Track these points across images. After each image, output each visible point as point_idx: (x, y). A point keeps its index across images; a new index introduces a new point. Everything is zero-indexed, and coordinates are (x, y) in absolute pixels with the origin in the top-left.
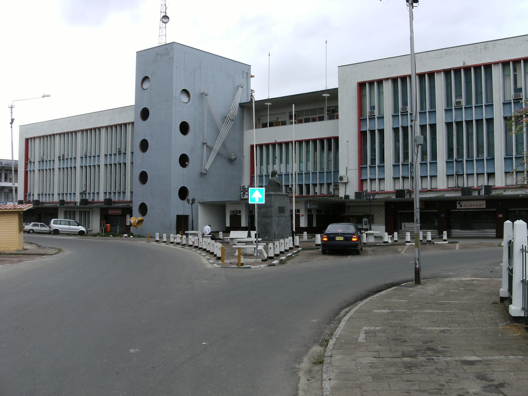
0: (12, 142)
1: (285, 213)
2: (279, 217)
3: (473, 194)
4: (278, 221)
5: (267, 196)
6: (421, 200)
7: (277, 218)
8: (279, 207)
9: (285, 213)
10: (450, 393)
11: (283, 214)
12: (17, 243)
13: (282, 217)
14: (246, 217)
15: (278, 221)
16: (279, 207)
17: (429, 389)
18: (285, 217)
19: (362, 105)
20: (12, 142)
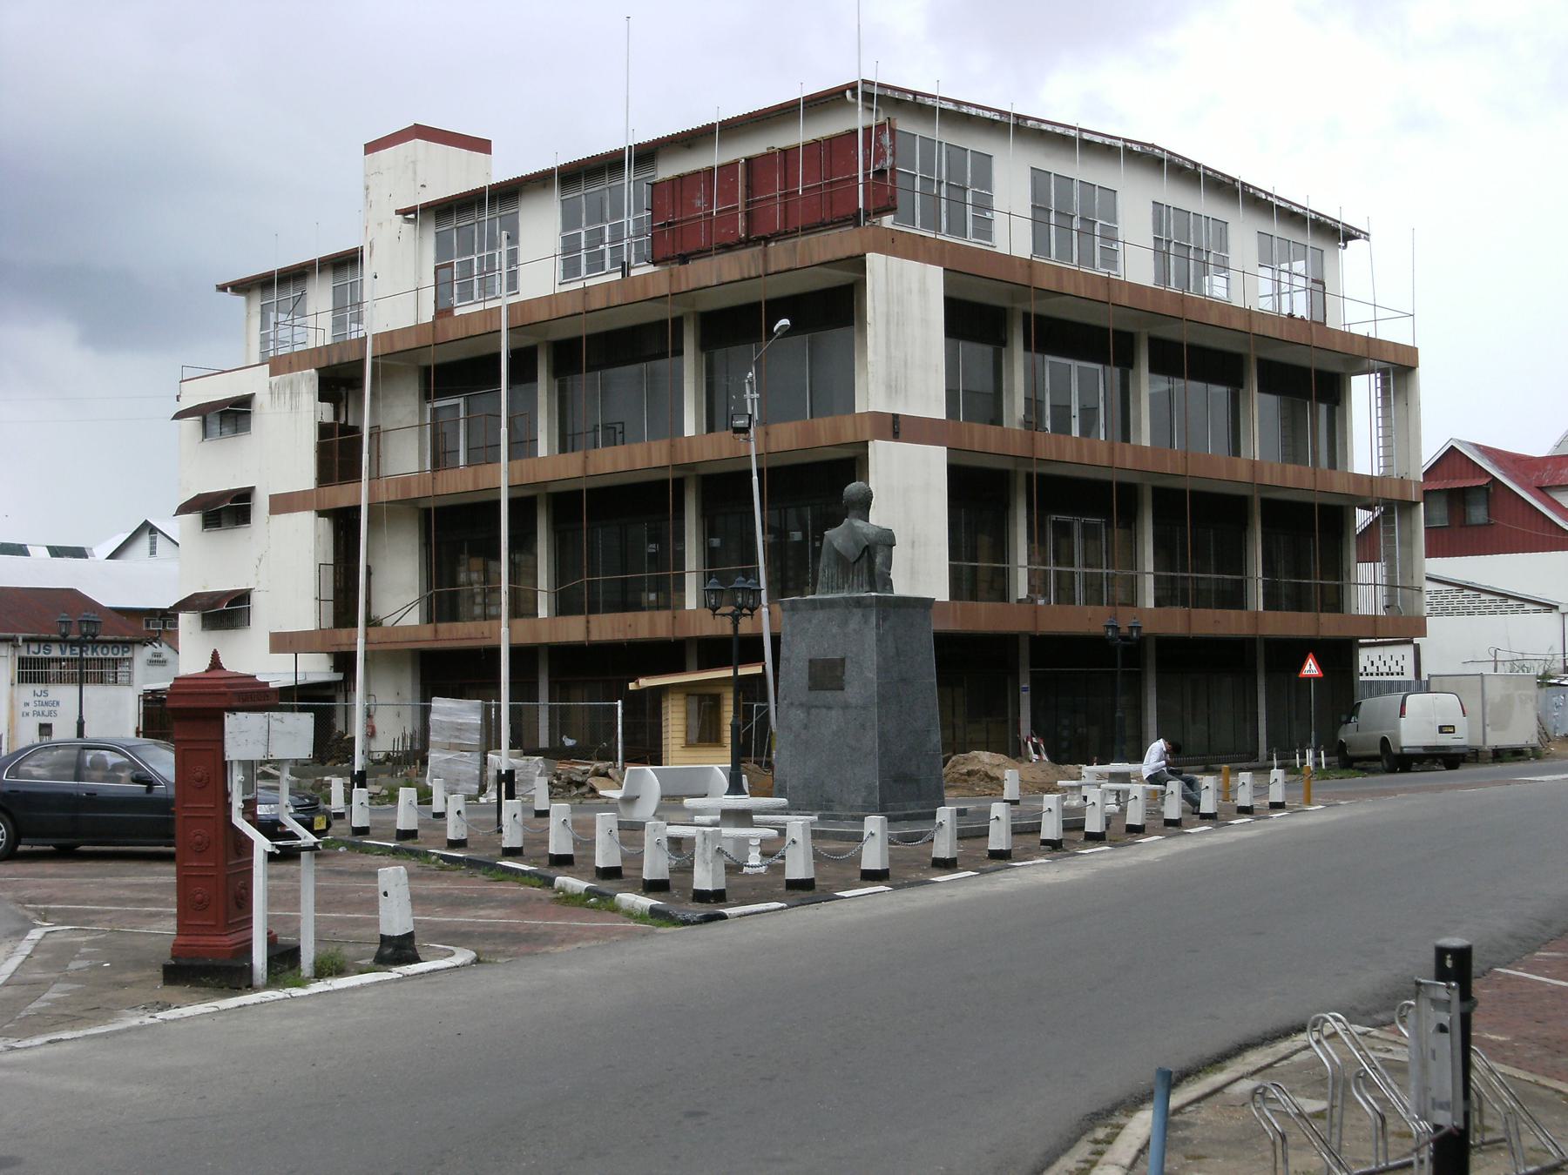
0: (628, 97)
1: (848, 689)
2: (808, 707)
3: (1272, 400)
4: (806, 727)
5: (721, 543)
6: (565, 605)
7: (800, 714)
8: (810, 661)
9: (843, 689)
10: (865, 1020)
11: (829, 696)
12: (673, 725)
13: (829, 708)
14: (413, 715)
15: (806, 727)
16: (810, 661)
17: (953, 758)
18: (846, 707)
19: (1059, 130)
20: (628, 97)
